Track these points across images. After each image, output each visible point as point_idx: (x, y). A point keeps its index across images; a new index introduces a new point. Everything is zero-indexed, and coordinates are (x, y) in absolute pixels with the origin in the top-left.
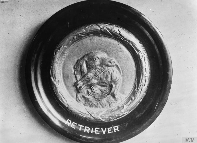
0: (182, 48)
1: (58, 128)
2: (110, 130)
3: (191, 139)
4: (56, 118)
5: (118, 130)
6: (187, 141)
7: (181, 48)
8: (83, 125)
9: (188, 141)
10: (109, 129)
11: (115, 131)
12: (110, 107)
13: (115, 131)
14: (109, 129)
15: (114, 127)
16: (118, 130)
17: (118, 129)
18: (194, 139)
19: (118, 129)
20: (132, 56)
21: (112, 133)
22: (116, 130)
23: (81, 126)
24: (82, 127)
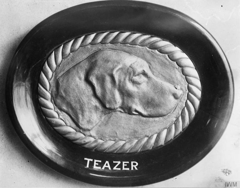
0: (212, 56)
1: (215, 119)
2: (126, 165)
3: (233, 183)
4: (45, 145)
5: (136, 169)
6: (228, 186)
7: (212, 55)
8: (89, 166)
9: (229, 185)
10: (125, 164)
11: (132, 169)
12: (161, 111)
13: (132, 169)
14: (125, 164)
15: (132, 162)
16: (136, 169)
17: (136, 167)
18: (236, 183)
19: (136, 167)
20: (99, 151)
21: (115, 161)
22: (134, 168)
23: (89, 160)
24: (90, 161)
